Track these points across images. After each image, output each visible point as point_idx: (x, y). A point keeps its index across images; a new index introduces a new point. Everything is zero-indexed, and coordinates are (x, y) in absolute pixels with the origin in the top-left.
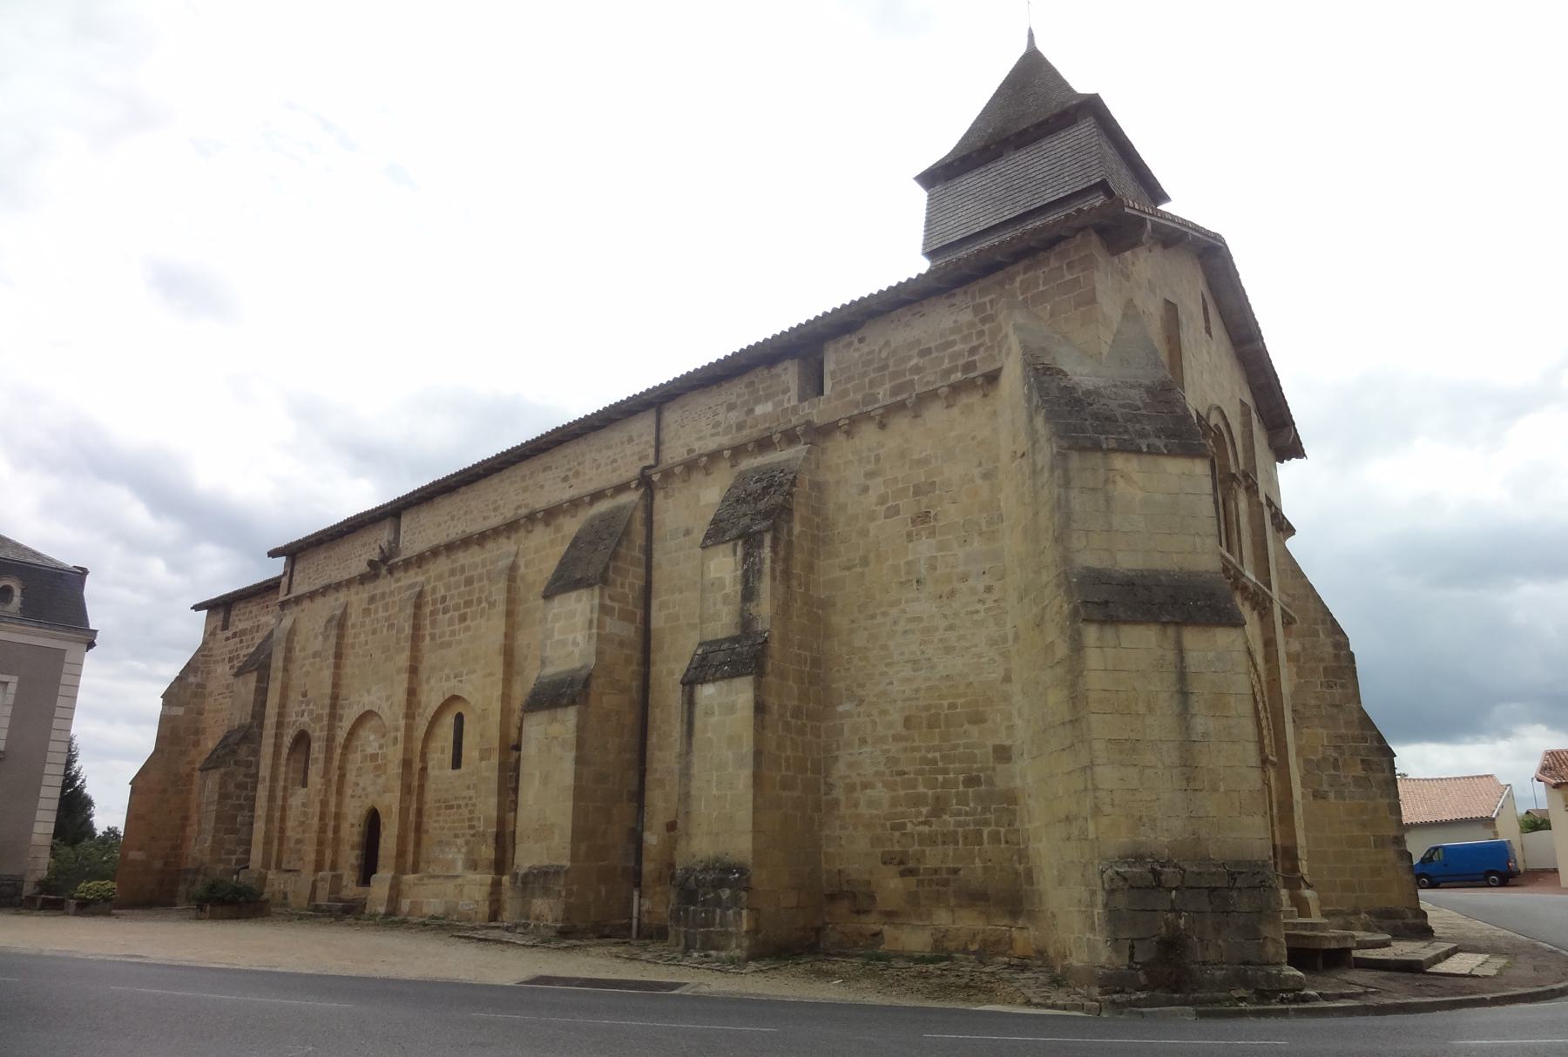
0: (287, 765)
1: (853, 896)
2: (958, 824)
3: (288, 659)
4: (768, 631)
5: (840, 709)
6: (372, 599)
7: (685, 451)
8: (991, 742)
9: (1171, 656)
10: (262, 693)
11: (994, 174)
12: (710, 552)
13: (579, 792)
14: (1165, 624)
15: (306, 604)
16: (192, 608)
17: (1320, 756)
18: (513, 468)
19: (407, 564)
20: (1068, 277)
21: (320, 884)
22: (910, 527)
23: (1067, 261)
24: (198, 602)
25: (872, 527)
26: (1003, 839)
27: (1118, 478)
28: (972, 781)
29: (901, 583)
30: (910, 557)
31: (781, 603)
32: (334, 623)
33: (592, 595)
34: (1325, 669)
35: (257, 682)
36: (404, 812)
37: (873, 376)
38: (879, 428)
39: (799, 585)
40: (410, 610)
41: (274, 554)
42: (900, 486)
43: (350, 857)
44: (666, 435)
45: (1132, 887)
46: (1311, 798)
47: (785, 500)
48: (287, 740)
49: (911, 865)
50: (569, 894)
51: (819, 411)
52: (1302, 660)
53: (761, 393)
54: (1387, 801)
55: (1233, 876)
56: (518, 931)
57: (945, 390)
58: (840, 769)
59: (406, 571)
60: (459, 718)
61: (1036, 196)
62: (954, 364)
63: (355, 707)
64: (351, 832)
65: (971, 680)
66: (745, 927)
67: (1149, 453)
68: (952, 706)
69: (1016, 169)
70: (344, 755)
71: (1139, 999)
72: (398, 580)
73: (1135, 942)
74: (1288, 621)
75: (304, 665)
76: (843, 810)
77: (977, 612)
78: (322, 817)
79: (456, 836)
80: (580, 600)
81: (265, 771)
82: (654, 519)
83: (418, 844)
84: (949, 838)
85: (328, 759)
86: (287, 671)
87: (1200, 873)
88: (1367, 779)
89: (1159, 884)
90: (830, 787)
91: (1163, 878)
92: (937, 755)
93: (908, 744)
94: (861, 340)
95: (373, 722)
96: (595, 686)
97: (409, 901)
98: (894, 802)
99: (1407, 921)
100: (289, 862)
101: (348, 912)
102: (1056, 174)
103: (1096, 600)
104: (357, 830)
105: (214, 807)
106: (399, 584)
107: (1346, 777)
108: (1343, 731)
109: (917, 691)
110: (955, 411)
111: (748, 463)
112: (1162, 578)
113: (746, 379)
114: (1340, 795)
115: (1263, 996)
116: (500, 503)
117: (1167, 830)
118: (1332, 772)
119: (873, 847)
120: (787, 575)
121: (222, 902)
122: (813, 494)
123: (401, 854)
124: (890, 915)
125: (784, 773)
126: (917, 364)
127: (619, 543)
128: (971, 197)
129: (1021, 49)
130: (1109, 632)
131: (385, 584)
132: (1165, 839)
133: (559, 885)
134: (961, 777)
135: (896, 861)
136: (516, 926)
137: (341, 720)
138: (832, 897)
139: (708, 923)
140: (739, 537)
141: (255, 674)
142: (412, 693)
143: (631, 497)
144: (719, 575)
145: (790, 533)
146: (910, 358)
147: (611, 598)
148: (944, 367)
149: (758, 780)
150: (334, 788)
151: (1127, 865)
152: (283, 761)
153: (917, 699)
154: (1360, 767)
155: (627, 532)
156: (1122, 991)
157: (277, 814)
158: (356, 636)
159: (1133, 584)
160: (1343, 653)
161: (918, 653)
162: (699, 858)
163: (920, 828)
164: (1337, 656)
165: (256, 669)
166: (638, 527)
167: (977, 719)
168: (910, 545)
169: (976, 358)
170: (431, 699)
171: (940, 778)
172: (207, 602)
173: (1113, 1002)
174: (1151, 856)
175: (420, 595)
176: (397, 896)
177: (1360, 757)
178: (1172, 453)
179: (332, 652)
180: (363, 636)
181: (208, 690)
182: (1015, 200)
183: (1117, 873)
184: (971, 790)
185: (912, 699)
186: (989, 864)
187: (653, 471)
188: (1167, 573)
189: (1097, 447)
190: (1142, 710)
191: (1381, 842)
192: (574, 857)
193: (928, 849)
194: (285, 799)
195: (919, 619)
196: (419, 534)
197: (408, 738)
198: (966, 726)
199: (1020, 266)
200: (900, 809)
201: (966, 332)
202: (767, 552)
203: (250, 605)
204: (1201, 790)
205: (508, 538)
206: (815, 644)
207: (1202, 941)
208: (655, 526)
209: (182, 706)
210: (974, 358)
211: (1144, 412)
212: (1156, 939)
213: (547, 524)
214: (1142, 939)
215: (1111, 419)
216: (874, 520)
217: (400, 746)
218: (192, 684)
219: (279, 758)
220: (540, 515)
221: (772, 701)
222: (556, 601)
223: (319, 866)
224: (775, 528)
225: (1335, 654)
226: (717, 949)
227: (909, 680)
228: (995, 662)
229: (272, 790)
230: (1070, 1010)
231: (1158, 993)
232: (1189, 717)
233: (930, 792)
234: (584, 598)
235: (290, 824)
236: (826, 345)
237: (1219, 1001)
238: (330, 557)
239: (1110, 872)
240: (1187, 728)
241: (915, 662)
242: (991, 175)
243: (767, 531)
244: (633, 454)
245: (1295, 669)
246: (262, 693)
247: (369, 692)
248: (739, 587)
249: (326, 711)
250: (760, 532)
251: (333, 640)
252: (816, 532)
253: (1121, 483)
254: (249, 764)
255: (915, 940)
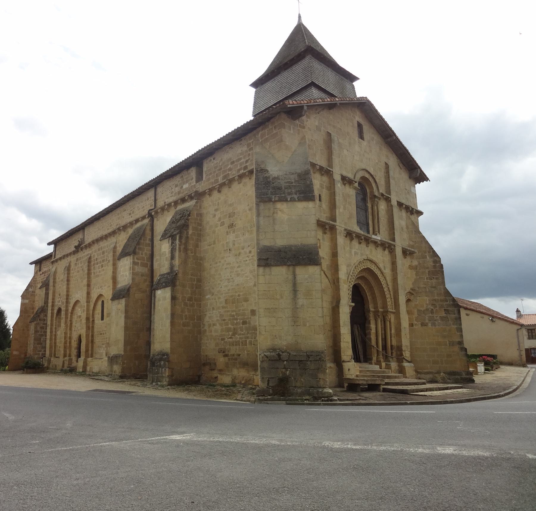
0: (56, 320)
1: (210, 364)
2: (240, 338)
3: (54, 282)
4: (178, 270)
5: (207, 297)
6: (77, 260)
7: (163, 202)
8: (250, 309)
9: (291, 277)
10: (47, 294)
11: (276, 81)
12: (162, 242)
13: (126, 328)
14: (289, 266)
15: (59, 262)
16: (30, 264)
17: (425, 308)
18: (115, 210)
19: (86, 247)
20: (275, 132)
21: (65, 362)
22: (227, 230)
23: (274, 126)
24: (31, 262)
25: (217, 229)
26: (253, 344)
27: (279, 211)
28: (244, 323)
29: (225, 250)
30: (227, 241)
31: (183, 260)
32: (66, 269)
33: (131, 258)
34: (429, 272)
35: (45, 290)
36: (87, 335)
37: (217, 172)
38: (218, 192)
39: (192, 252)
40: (87, 264)
41: (49, 244)
42: (225, 214)
43: (74, 352)
44: (158, 197)
45: (269, 360)
46: (420, 326)
47: (185, 222)
48: (55, 311)
49: (226, 353)
50: (123, 363)
51: (201, 187)
52: (418, 269)
53: (185, 180)
54: (456, 326)
55: (308, 356)
56: (110, 376)
57: (237, 177)
58: (207, 319)
59: (86, 249)
60: (103, 302)
61: (290, 90)
62: (241, 167)
63: (74, 299)
64: (74, 344)
65: (244, 286)
66: (167, 374)
67: (291, 201)
68: (239, 295)
69: (284, 79)
70: (71, 316)
71: (268, 398)
72: (84, 253)
73: (270, 379)
74: (405, 252)
75: (59, 284)
76: (207, 334)
77: (247, 261)
78: (65, 338)
79: (103, 344)
80: (127, 260)
81: (49, 323)
82: (154, 228)
83: (92, 347)
84: (237, 343)
85: (66, 318)
86: (55, 286)
87: (296, 355)
88: (447, 317)
89: (280, 359)
90: (204, 325)
91: (281, 357)
92: (234, 313)
93: (227, 309)
94: (214, 159)
95: (79, 305)
96: (132, 291)
97: (89, 367)
98: (222, 330)
99: (462, 376)
100: (58, 354)
101: (71, 371)
102: (297, 80)
103: (264, 258)
104: (76, 342)
105: (33, 335)
106: (84, 254)
107: (436, 317)
108: (436, 298)
109: (229, 290)
110: (241, 185)
111: (180, 207)
112: (293, 248)
113: (180, 175)
114: (434, 324)
115: (316, 399)
116: (112, 223)
117: (285, 340)
118: (430, 315)
119: (216, 346)
120: (186, 250)
121: (30, 368)
122: (198, 218)
123: (87, 351)
124: (220, 370)
125: (184, 320)
126: (230, 167)
127: (140, 239)
128: (269, 92)
129: (295, 24)
130: (267, 270)
131: (81, 254)
132: (285, 343)
133: (120, 361)
134: (241, 321)
135: (222, 352)
136: (109, 375)
137: (70, 304)
138: (204, 365)
139: (158, 373)
140: (170, 237)
141: (45, 287)
142: (88, 294)
143: (146, 221)
144: (165, 250)
145: (188, 233)
146: (228, 165)
147: (137, 259)
148: (238, 168)
149: (172, 323)
150: (69, 328)
151: (269, 352)
152: (54, 319)
153: (229, 293)
154: (444, 313)
155: (144, 234)
156: (264, 396)
157: (54, 337)
158: (73, 273)
159: (281, 251)
160: (437, 265)
161: (230, 276)
162: (157, 350)
163: (229, 340)
164: (435, 267)
165: (45, 286)
166: (148, 232)
167: (246, 300)
168: (228, 236)
169: (248, 164)
170: (94, 296)
171: (235, 321)
172: (35, 261)
173: (259, 399)
174: (279, 349)
175: (90, 258)
176: (86, 366)
177: (443, 308)
178: (300, 200)
179: (66, 279)
180: (75, 273)
181: (36, 294)
182: (308, 79)
183: (265, 355)
184: (244, 326)
185: (227, 293)
186: (249, 352)
187: (152, 211)
188: (295, 246)
189: (270, 200)
190: (278, 297)
191: (452, 344)
192: (125, 351)
193: (231, 347)
194: (56, 332)
195: (230, 264)
196: (91, 234)
197: (88, 310)
198: (243, 303)
199: (261, 128)
200: (224, 333)
201: (245, 154)
202: (177, 242)
203: (47, 262)
204: (299, 326)
205: (114, 236)
206: (199, 274)
207: (295, 379)
208: (154, 232)
209: (27, 299)
210: (247, 164)
211: (294, 184)
212: (277, 378)
213: (124, 231)
214: (272, 378)
215: (280, 188)
216: (217, 227)
217: (85, 312)
218: (30, 291)
219: (53, 317)
220: (121, 228)
221: (179, 296)
222: (121, 260)
223: (65, 356)
224: (180, 233)
225: (434, 265)
226: (160, 382)
227: (226, 286)
228: (251, 279)
229: (51, 329)
230: (247, 402)
231: (276, 397)
232: (296, 299)
233: (232, 327)
234: (128, 259)
235: (58, 341)
236: (204, 161)
237: (297, 400)
238: (66, 244)
239: (262, 355)
240: (295, 303)
241: (228, 279)
242: (275, 82)
243: (177, 234)
244: (149, 204)
245: (415, 273)
246: (47, 294)
247: (77, 293)
248: (170, 255)
249: (65, 301)
250: (175, 235)
251: (66, 275)
252: (200, 232)
253: (279, 213)
254: (44, 320)
255: (226, 379)
